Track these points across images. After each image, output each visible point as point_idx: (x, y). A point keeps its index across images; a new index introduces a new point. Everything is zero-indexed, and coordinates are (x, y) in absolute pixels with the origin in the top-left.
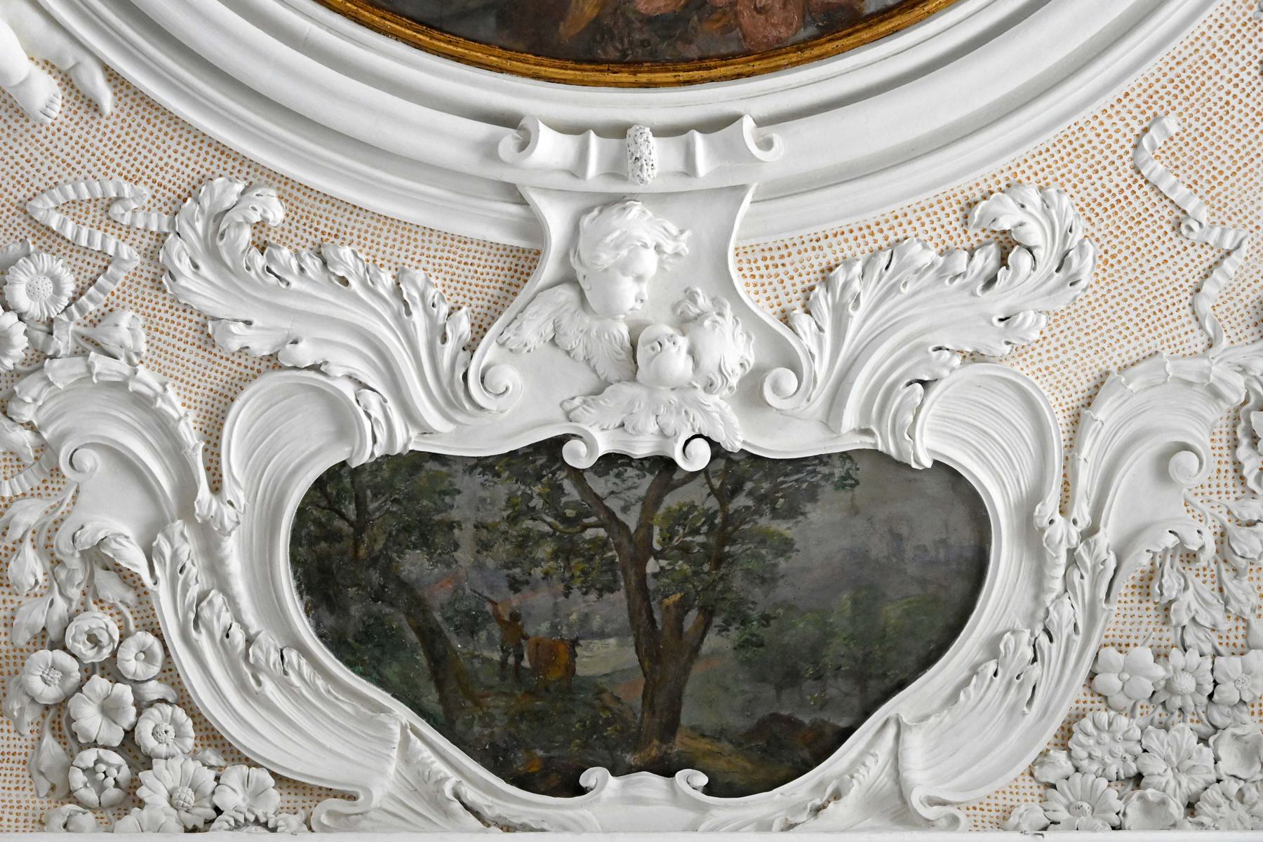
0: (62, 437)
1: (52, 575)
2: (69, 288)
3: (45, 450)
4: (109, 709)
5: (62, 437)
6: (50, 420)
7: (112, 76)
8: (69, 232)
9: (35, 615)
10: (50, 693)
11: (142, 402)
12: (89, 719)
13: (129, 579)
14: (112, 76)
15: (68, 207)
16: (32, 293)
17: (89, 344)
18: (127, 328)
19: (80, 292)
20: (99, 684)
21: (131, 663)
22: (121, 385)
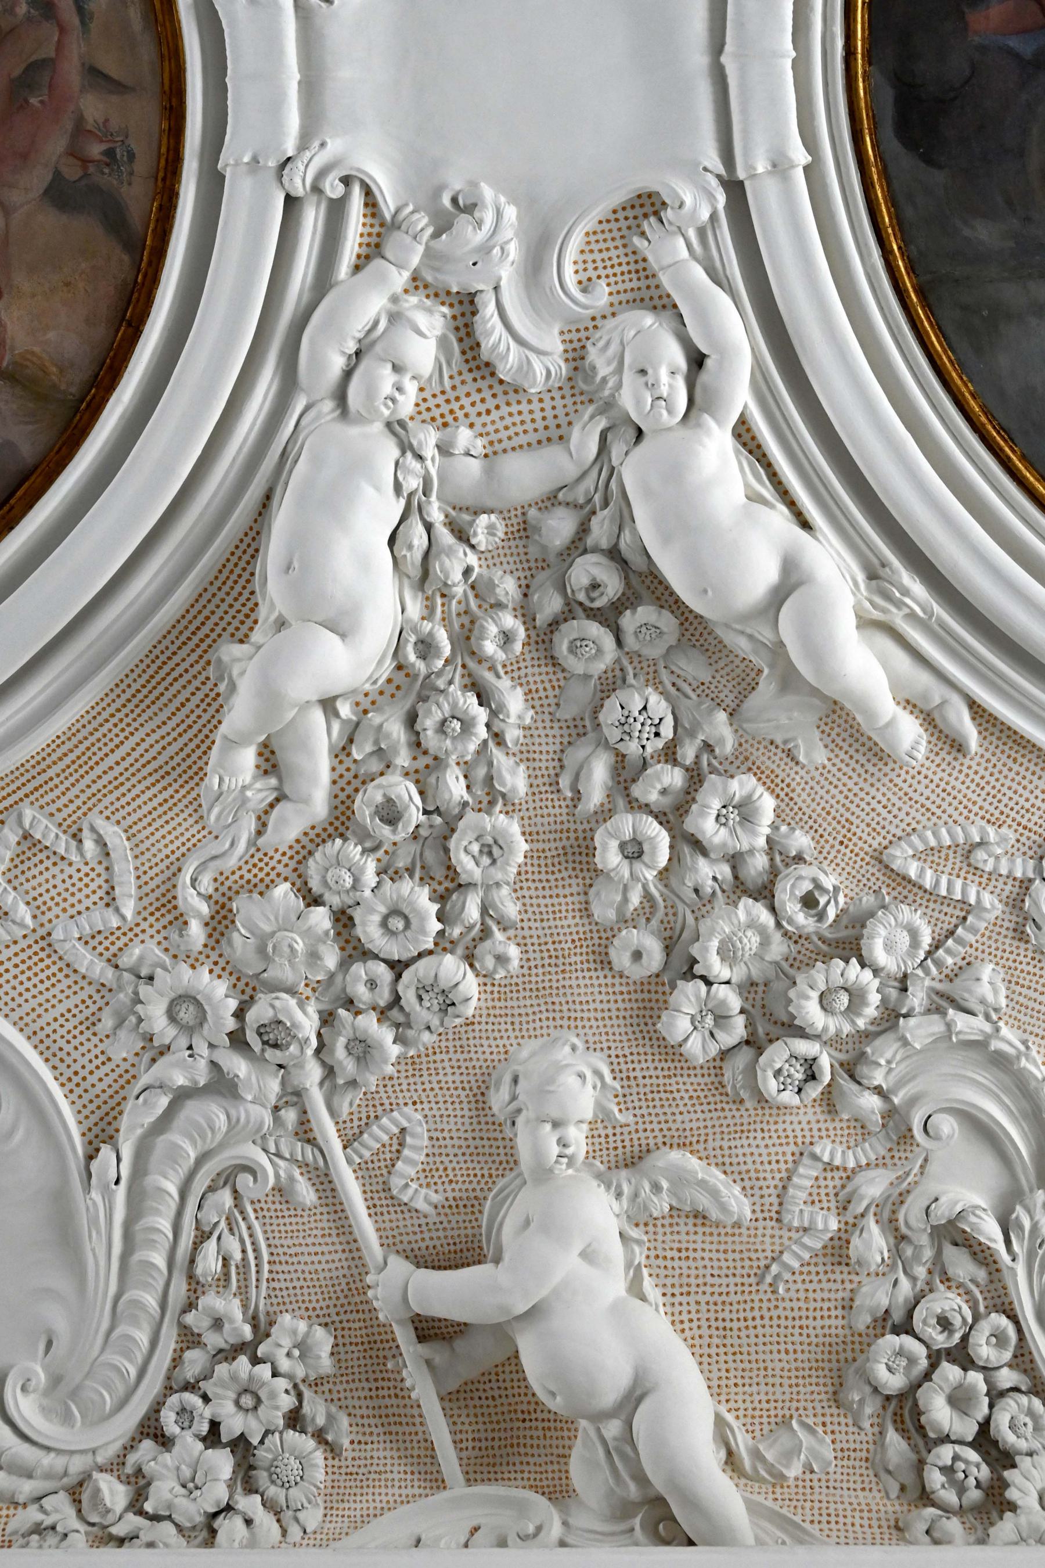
0: (913, 1101)
1: (896, 1251)
2: (926, 940)
3: (891, 1113)
4: (959, 1400)
5: (913, 1101)
6: (901, 1083)
7: (976, 708)
8: (928, 882)
9: (878, 1296)
10: (894, 1382)
11: (1001, 1062)
12: (939, 1412)
13: (981, 1255)
14: (976, 708)
15: (927, 855)
16: (889, 947)
17: (945, 1001)
18: (988, 983)
19: (937, 946)
20: (950, 1372)
21: (984, 1350)
22: (979, 1045)
